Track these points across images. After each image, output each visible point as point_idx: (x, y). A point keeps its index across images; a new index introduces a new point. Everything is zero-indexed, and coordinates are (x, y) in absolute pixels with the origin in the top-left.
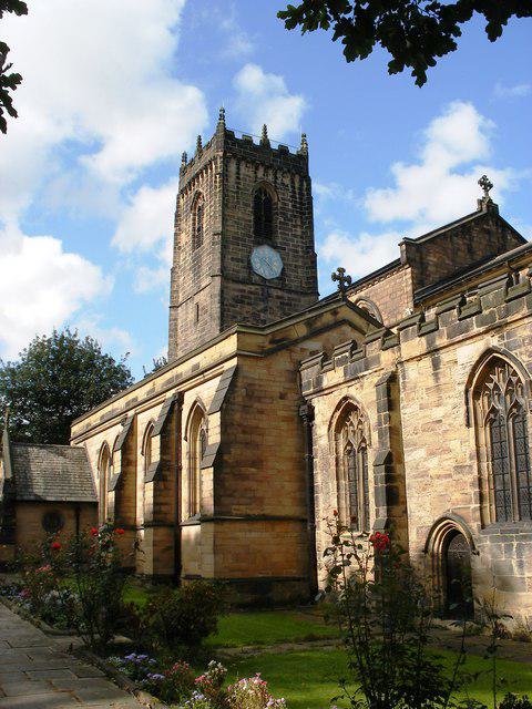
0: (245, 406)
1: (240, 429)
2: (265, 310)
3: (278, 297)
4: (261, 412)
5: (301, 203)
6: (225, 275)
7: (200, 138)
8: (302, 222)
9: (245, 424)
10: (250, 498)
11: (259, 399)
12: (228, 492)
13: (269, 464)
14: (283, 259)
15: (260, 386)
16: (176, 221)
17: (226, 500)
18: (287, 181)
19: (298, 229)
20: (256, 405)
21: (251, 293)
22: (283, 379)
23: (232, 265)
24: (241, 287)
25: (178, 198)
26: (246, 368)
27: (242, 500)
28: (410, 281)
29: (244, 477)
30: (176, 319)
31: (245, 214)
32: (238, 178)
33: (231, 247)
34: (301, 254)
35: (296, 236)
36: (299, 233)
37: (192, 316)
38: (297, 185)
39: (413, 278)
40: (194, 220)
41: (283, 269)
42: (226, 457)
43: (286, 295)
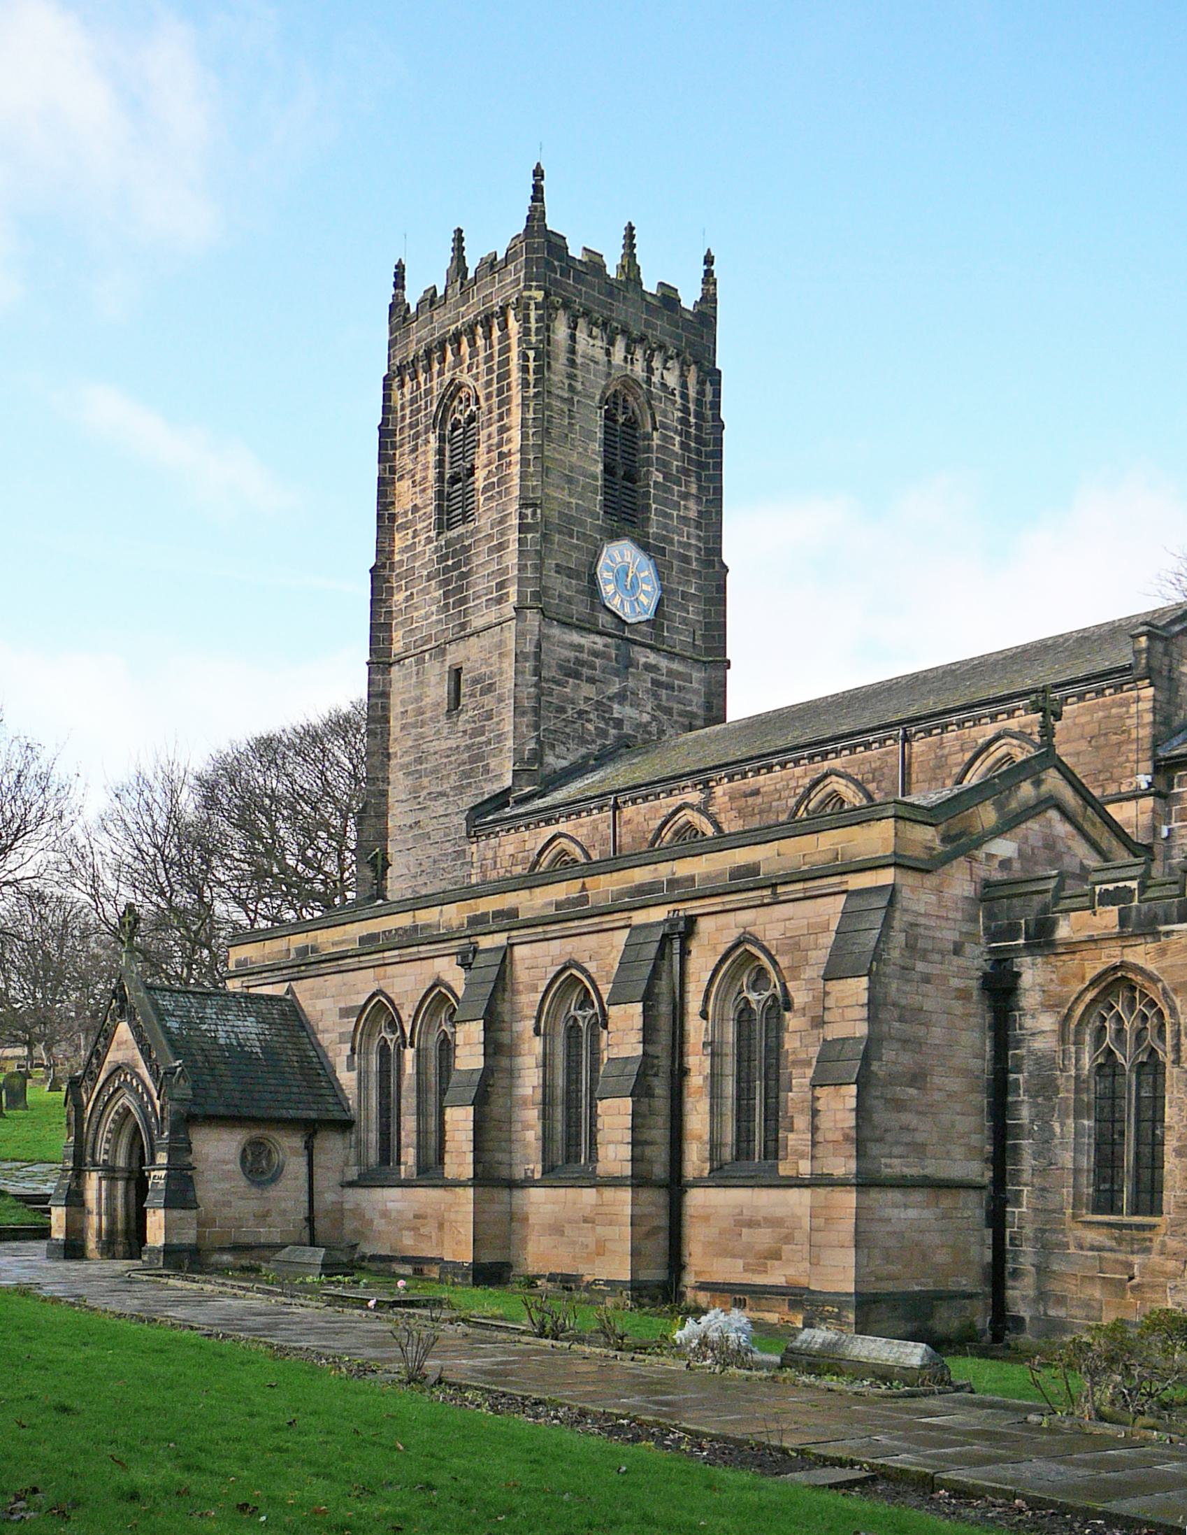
0: (904, 968)
1: (896, 1013)
2: (621, 697)
3: (649, 668)
4: (927, 979)
5: (698, 440)
6: (538, 602)
7: (459, 236)
8: (700, 488)
9: (903, 1002)
10: (907, 1144)
11: (924, 955)
12: (878, 1133)
13: (936, 1080)
14: (660, 577)
15: (927, 928)
16: (382, 445)
17: (639, 1121)
18: (672, 380)
19: (692, 504)
20: (920, 966)
21: (595, 654)
22: (959, 916)
23: (558, 584)
24: (575, 638)
25: (387, 386)
26: (905, 893)
27: (897, 1150)
28: (1149, 718)
29: (899, 1105)
30: (385, 695)
31: (587, 456)
32: (572, 363)
33: (557, 537)
34: (694, 565)
35: (684, 520)
36: (693, 514)
37: (438, 692)
38: (692, 393)
39: (1154, 710)
40: (440, 451)
41: (660, 603)
42: (875, 1066)
43: (664, 663)
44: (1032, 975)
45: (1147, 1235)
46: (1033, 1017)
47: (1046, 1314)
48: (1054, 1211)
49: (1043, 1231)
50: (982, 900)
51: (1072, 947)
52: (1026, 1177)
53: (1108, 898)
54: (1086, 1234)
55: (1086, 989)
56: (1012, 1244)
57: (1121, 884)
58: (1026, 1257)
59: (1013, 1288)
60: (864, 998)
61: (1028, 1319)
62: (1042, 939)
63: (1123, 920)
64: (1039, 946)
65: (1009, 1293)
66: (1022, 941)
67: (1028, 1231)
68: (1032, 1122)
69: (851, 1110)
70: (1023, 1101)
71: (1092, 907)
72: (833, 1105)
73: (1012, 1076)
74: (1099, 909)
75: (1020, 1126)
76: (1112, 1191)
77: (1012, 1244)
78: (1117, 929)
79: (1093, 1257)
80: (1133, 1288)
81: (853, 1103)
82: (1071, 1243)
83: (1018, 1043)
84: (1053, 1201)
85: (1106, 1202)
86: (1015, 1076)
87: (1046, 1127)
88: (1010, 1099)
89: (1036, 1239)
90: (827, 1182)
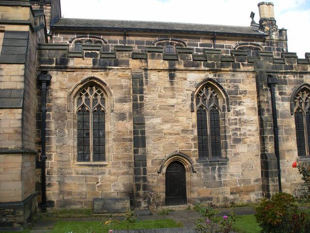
44: (57, 78)
45: (103, 168)
46: (56, 92)
47: (63, 199)
48: (65, 161)
49: (62, 169)
50: (38, 49)
51: (74, 69)
52: (53, 149)
53: (88, 55)
54: (76, 167)
55: (79, 84)
56: (48, 174)
57: (93, 51)
58: (54, 179)
59: (49, 190)
60: (22, 73)
61: (55, 202)
62: (62, 66)
63: (94, 62)
64: (61, 68)
65: (47, 192)
66: (54, 65)
67: (55, 169)
68: (56, 129)
69: (19, 119)
70: (51, 122)
71: (82, 57)
72: (8, 117)
73: (47, 113)
74: (85, 58)
75: (51, 131)
76: (84, 154)
77: (48, 174)
78: (92, 65)
79: (83, 177)
80: (99, 186)
81: (20, 117)
82: (74, 172)
83: (50, 101)
84: (65, 158)
85: (82, 156)
86: (49, 113)
87: (62, 131)
88: (46, 121)
89: (59, 172)
90: (6, 151)
